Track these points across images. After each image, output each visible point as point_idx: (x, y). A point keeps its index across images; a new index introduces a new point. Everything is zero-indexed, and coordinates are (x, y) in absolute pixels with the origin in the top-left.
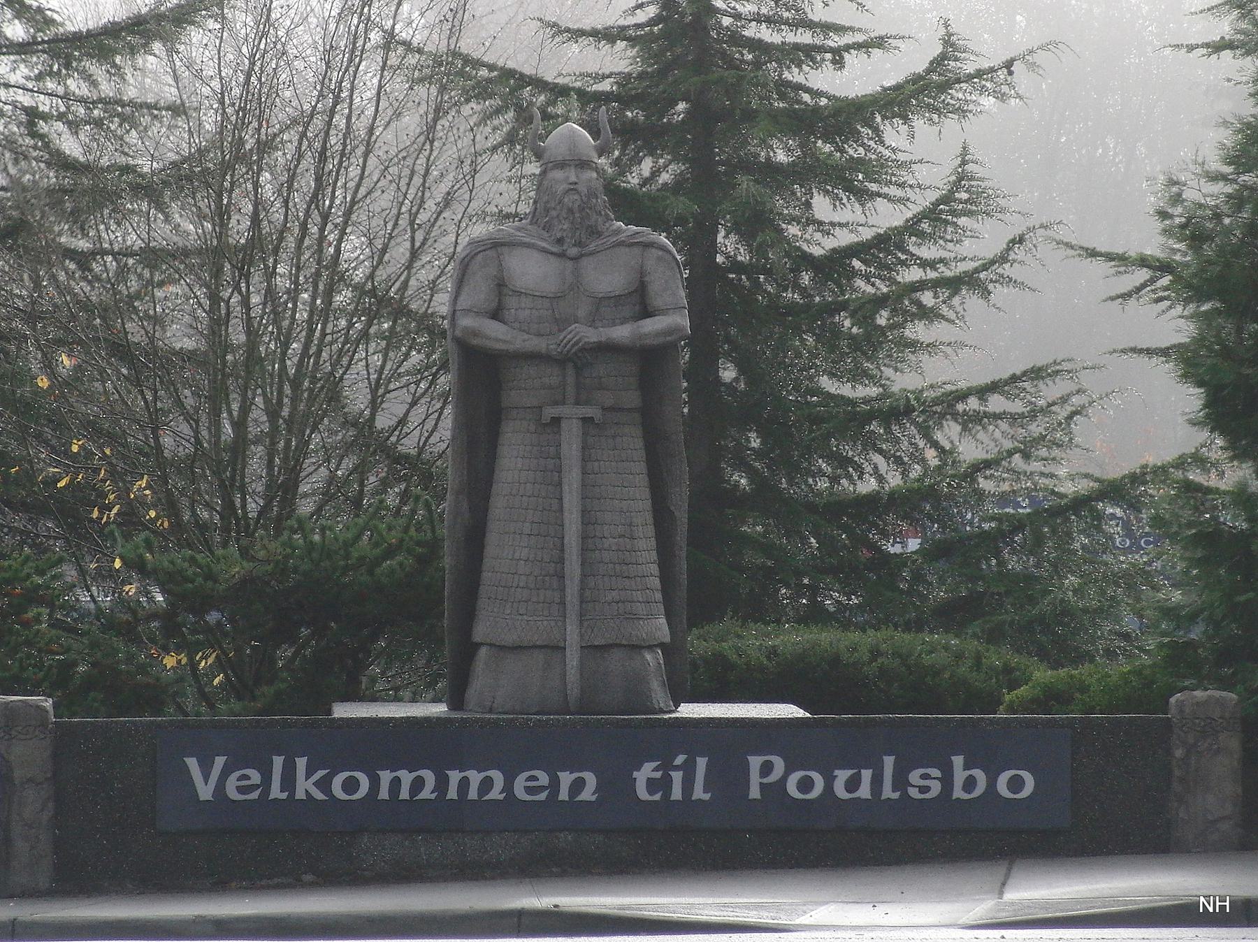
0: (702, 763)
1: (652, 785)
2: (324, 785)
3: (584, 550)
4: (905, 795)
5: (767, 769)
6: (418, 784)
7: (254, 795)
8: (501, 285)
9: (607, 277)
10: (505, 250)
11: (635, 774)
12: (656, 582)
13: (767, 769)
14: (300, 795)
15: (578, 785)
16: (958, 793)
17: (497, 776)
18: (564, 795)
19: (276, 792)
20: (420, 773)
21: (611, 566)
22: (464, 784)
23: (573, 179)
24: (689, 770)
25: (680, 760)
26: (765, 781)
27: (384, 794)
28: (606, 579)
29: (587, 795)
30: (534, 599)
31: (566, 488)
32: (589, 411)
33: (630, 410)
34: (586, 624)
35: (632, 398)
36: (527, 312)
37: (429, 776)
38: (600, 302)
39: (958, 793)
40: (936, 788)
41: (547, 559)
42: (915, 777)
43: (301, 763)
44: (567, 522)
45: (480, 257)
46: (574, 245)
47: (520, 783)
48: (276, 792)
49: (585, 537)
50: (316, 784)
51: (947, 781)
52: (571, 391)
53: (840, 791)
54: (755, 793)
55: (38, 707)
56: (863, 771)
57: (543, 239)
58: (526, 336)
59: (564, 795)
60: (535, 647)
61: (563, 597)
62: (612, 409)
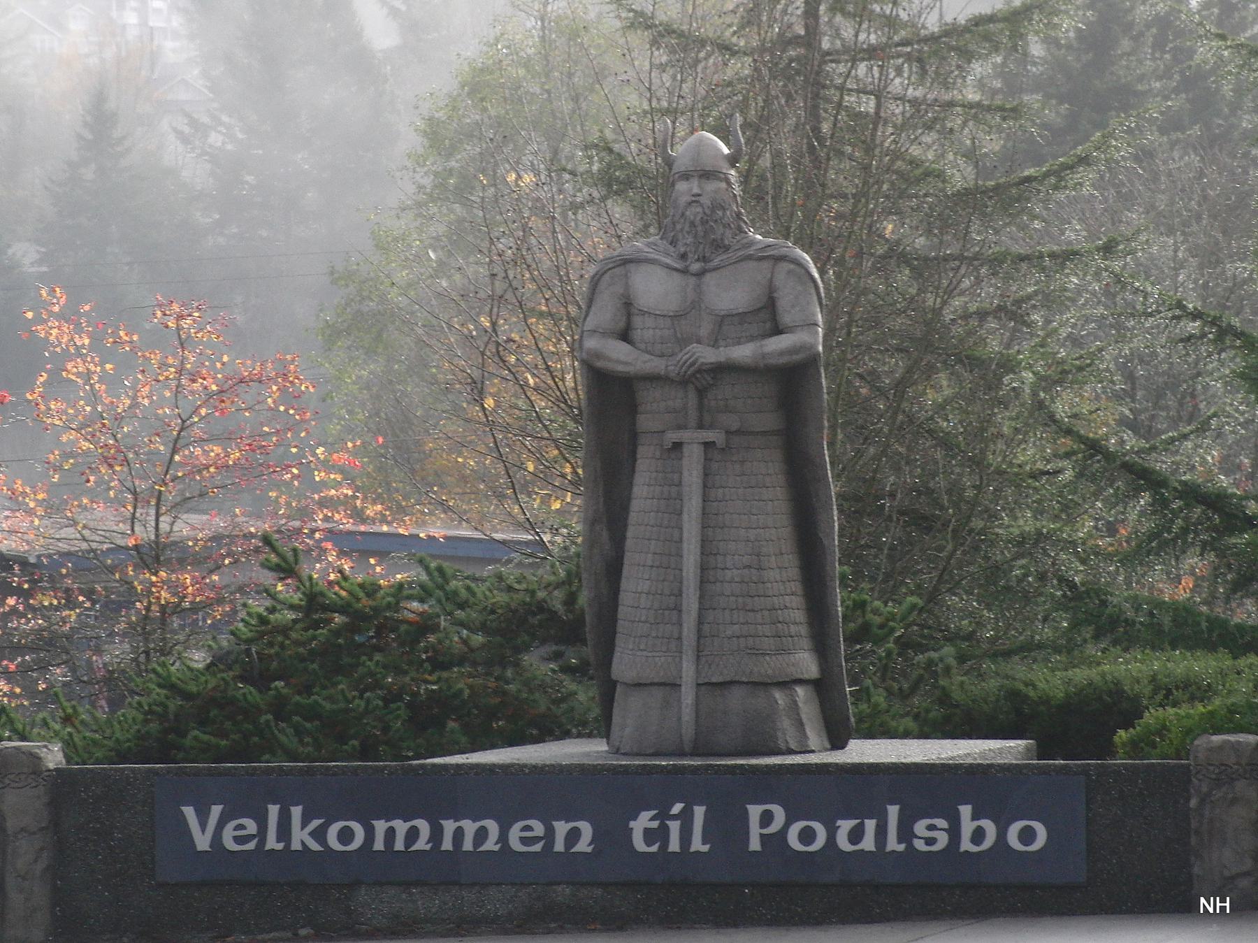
0: (699, 812)
1: (649, 835)
2: (319, 835)
3: (703, 582)
4: (910, 846)
5: (767, 818)
6: (413, 834)
7: (251, 846)
8: (628, 305)
9: (730, 293)
10: (632, 267)
11: (632, 824)
12: (799, 615)
13: (767, 818)
14: (295, 845)
15: (574, 836)
16: (966, 845)
17: (492, 826)
18: (559, 846)
19: (272, 843)
20: (483, 823)
21: (733, 599)
22: (459, 834)
23: (696, 190)
24: (686, 818)
25: (677, 808)
26: (765, 831)
27: (379, 845)
28: (727, 612)
29: (583, 846)
30: (654, 634)
31: (685, 516)
32: (710, 436)
33: (764, 433)
34: (704, 659)
35: (769, 420)
36: (651, 332)
37: (423, 826)
38: (723, 320)
39: (966, 845)
40: (943, 840)
41: (667, 592)
42: (920, 827)
43: (296, 812)
44: (685, 552)
45: (607, 277)
46: (698, 260)
47: (515, 833)
48: (272, 843)
49: (704, 568)
50: (311, 834)
51: (954, 832)
52: (693, 414)
53: (843, 843)
54: (755, 845)
55: (31, 754)
56: (866, 821)
57: (668, 254)
58: (648, 357)
59: (559, 846)
60: (652, 684)
61: (680, 633)
62: (739, 432)
